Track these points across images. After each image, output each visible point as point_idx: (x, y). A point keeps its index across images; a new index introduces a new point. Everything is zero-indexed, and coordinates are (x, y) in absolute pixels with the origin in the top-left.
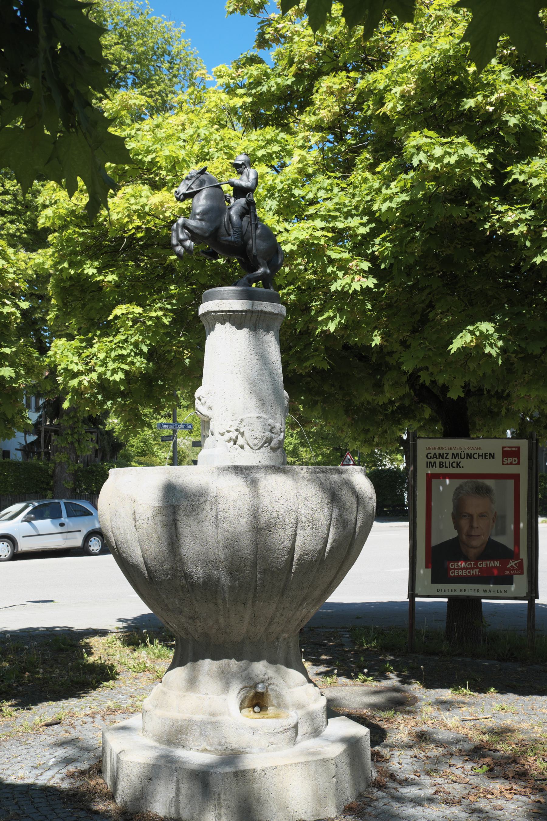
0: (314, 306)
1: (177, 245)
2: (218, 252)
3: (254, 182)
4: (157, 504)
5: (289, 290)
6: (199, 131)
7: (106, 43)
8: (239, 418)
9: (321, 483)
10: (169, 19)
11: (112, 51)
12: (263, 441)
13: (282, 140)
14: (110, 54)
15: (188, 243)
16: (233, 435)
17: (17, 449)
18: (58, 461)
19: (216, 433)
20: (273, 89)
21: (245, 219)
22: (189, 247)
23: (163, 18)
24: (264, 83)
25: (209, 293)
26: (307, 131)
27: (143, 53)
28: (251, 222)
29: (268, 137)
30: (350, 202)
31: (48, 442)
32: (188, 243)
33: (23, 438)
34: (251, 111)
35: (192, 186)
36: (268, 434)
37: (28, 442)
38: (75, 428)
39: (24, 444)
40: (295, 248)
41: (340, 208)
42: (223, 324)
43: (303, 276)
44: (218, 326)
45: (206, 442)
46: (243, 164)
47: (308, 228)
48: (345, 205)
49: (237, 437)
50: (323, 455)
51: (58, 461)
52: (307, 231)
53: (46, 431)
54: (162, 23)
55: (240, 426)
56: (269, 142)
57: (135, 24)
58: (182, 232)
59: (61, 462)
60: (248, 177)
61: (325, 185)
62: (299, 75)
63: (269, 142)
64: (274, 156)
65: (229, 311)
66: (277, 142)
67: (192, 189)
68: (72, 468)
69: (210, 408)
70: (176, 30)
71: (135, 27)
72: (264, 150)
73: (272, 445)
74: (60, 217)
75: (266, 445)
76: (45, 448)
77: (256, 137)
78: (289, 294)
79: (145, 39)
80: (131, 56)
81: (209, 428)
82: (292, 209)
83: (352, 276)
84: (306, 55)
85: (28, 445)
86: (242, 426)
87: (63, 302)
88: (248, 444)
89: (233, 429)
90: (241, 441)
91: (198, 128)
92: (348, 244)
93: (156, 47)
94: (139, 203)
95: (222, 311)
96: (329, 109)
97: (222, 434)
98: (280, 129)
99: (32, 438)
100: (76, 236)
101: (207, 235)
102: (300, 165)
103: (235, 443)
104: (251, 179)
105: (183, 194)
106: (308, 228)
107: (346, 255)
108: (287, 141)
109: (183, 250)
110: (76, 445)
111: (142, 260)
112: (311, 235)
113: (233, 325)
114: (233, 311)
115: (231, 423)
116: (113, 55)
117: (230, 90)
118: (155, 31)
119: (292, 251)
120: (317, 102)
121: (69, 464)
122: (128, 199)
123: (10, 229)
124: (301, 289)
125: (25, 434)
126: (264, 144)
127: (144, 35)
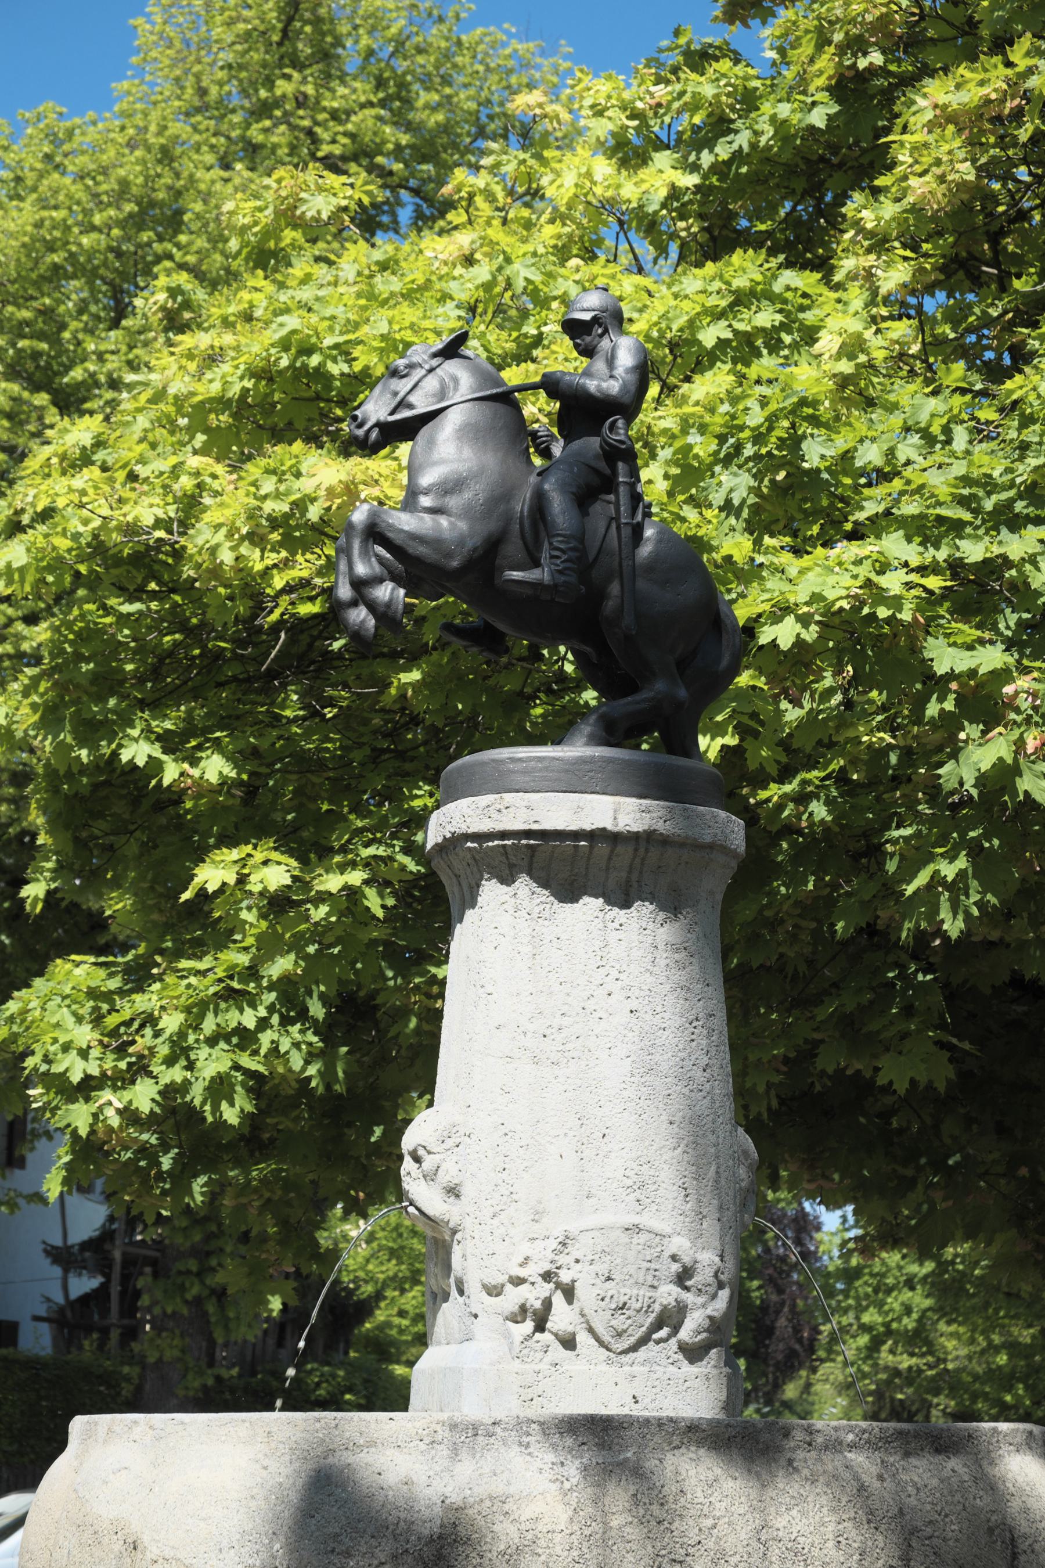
0: (894, 842)
1: (354, 604)
2: (501, 626)
3: (632, 378)
4: (573, 1471)
5: (805, 782)
6: (508, 271)
7: (335, 104)
8: (558, 1232)
9: (862, 1488)
10: (525, 36)
11: (350, 127)
12: (651, 1318)
13: (789, 295)
14: (345, 134)
15: (384, 592)
16: (533, 1295)
17: (37, 1318)
18: (152, 1358)
19: (473, 1287)
20: (763, 140)
21: (597, 508)
22: (389, 604)
23: (506, 32)
24: (739, 124)
25: (459, 770)
26: (869, 251)
27: (445, 128)
28: (617, 518)
29: (740, 282)
30: (1008, 470)
31: (130, 1298)
32: (384, 592)
33: (58, 1284)
34: (701, 216)
35: (412, 399)
36: (668, 1293)
37: (74, 1294)
38: (208, 1254)
39: (60, 1299)
40: (810, 635)
41: (973, 496)
42: (507, 880)
43: (851, 733)
44: (491, 891)
45: (440, 1316)
46: (595, 319)
47: (858, 562)
48: (989, 485)
49: (548, 1304)
50: (1012, 1347)
51: (152, 1358)
52: (856, 570)
53: (129, 1262)
54: (504, 45)
55: (562, 1260)
56: (741, 300)
57: (420, 51)
58: (365, 553)
59: (160, 1360)
60: (611, 362)
61: (924, 418)
62: (848, 87)
63: (741, 300)
64: (759, 342)
65: (528, 834)
66: (771, 297)
67: (411, 406)
68: (197, 1384)
69: (453, 1191)
70: (546, 63)
71: (420, 59)
72: (723, 323)
73: (686, 1333)
74: (57, 564)
75: (663, 1333)
76: (122, 1315)
77: (699, 285)
78: (802, 798)
79: (448, 91)
80: (405, 139)
81: (448, 1267)
82: (803, 505)
83: (1016, 734)
84: (869, 18)
85: (71, 1304)
86: (570, 1260)
87: (76, 840)
88: (591, 1330)
89: (532, 1271)
90: (562, 1317)
91: (508, 260)
92: (1009, 620)
93: (484, 112)
94: (288, 493)
95: (503, 835)
96: (938, 171)
97: (494, 1291)
98: (781, 258)
99: (83, 1284)
100: (108, 620)
101: (455, 564)
102: (846, 367)
103: (540, 1327)
104: (619, 371)
105: (378, 424)
106: (858, 562)
107: (992, 658)
108: (805, 295)
109: (372, 622)
110: (211, 1308)
111: (331, 703)
112: (868, 584)
113: (544, 884)
114: (543, 835)
115: (526, 1249)
116: (352, 136)
117: (630, 154)
118: (481, 68)
119: (799, 643)
120: (904, 157)
121: (187, 1369)
122: (254, 484)
123: (25, 638)
124: (848, 781)
125: (66, 1271)
126: (724, 303)
127: (446, 81)
